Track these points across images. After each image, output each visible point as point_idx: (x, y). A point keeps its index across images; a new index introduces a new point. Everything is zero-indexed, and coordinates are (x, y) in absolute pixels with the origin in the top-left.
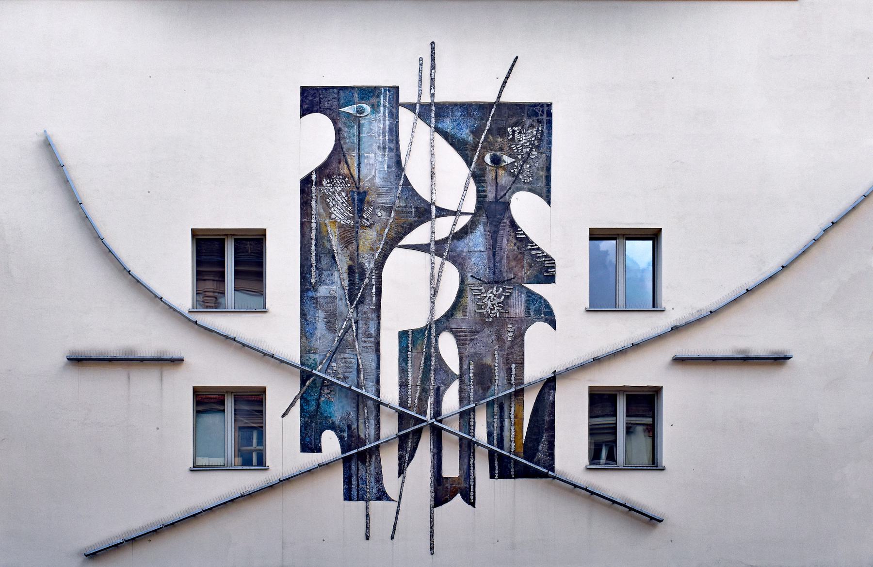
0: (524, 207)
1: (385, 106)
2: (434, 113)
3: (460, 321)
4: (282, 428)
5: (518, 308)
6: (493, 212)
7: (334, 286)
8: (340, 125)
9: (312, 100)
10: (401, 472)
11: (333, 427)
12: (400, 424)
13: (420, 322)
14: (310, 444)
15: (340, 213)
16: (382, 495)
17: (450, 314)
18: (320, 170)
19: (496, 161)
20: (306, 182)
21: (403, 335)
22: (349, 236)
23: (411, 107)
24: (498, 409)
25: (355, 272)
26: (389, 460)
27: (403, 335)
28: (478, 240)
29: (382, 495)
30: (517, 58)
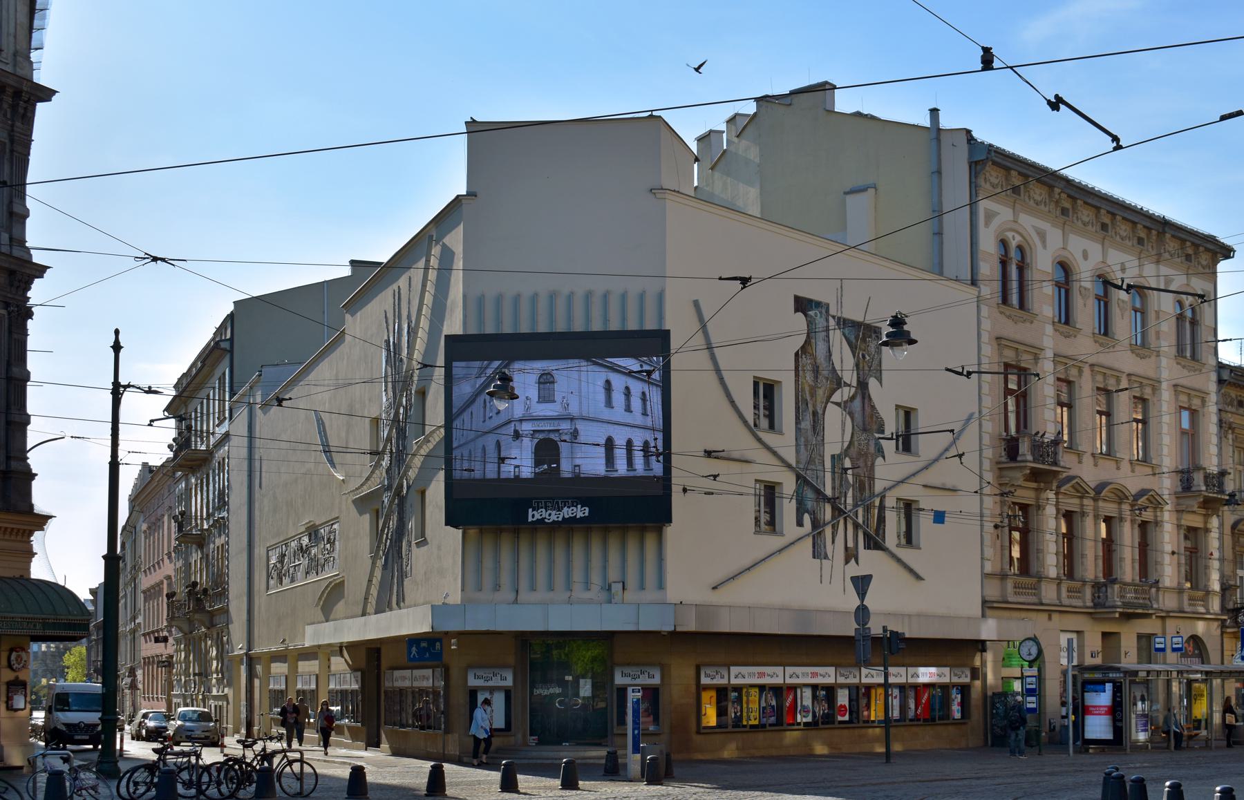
0: (873, 383)
1: (413, 679)
2: (843, 323)
3: (853, 451)
4: (788, 509)
5: (872, 449)
6: (863, 386)
7: (806, 424)
8: (421, 601)
9: (802, 305)
10: (833, 542)
11: (807, 512)
12: (856, 325)
13: (838, 452)
14: (800, 523)
15: (809, 377)
16: (826, 557)
17: (849, 447)
18: (803, 347)
19: (864, 356)
20: (797, 354)
21: (833, 456)
22: (813, 395)
23: (834, 317)
24: (868, 510)
25: (815, 413)
26: (828, 531)
27: (833, 456)
28: (857, 403)
29: (826, 557)
30: (919, 577)
